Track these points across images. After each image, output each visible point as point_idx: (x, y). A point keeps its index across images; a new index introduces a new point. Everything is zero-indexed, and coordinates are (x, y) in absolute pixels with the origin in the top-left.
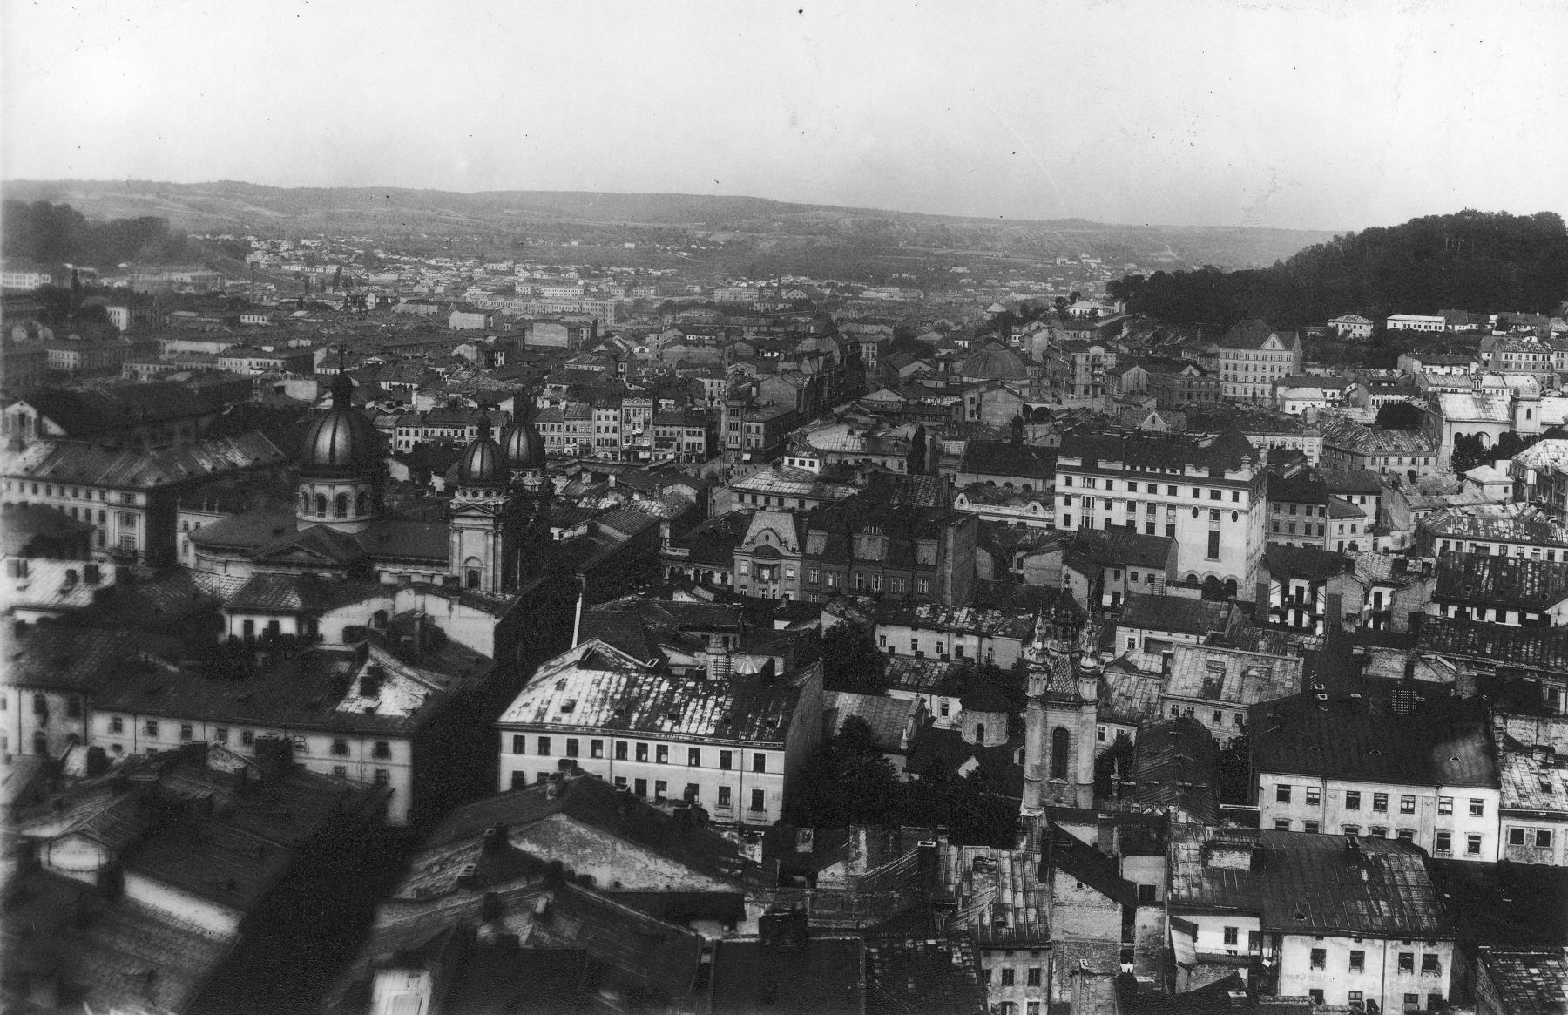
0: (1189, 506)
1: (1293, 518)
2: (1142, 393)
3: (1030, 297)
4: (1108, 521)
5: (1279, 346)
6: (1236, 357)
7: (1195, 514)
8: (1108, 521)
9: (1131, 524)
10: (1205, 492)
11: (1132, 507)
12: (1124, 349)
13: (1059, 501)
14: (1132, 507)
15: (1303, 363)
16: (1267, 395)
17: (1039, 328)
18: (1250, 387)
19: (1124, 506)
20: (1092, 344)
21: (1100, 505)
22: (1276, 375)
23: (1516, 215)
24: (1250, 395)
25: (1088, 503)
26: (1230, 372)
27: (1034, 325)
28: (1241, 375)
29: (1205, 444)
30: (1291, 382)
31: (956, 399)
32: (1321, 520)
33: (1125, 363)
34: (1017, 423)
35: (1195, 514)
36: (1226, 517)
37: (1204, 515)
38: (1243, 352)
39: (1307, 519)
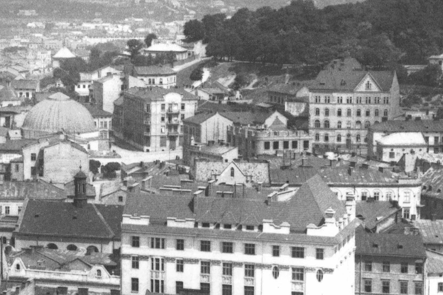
0: (269, 267)
1: (386, 276)
2: (221, 143)
3: (104, 41)
4: (179, 284)
5: (374, 88)
6: (328, 101)
7: (276, 275)
8: (179, 284)
9: (205, 288)
10: (286, 250)
11: (206, 267)
12: (204, 96)
13: (126, 264)
14: (206, 267)
15: (406, 104)
16: (362, 142)
17: (109, 74)
18: (344, 133)
19: (197, 267)
20: (167, 92)
21: (170, 267)
22: (372, 119)
23: (277, 7)
24: (343, 141)
25: (158, 265)
26: (322, 117)
27: (104, 72)
28: (333, 120)
29: (283, 198)
30: (390, 126)
31: (17, 156)
32: (418, 278)
33: (205, 110)
34: (79, 180)
35: (276, 275)
36: (310, 277)
37: (286, 276)
38: (336, 95)
39: (402, 277)
